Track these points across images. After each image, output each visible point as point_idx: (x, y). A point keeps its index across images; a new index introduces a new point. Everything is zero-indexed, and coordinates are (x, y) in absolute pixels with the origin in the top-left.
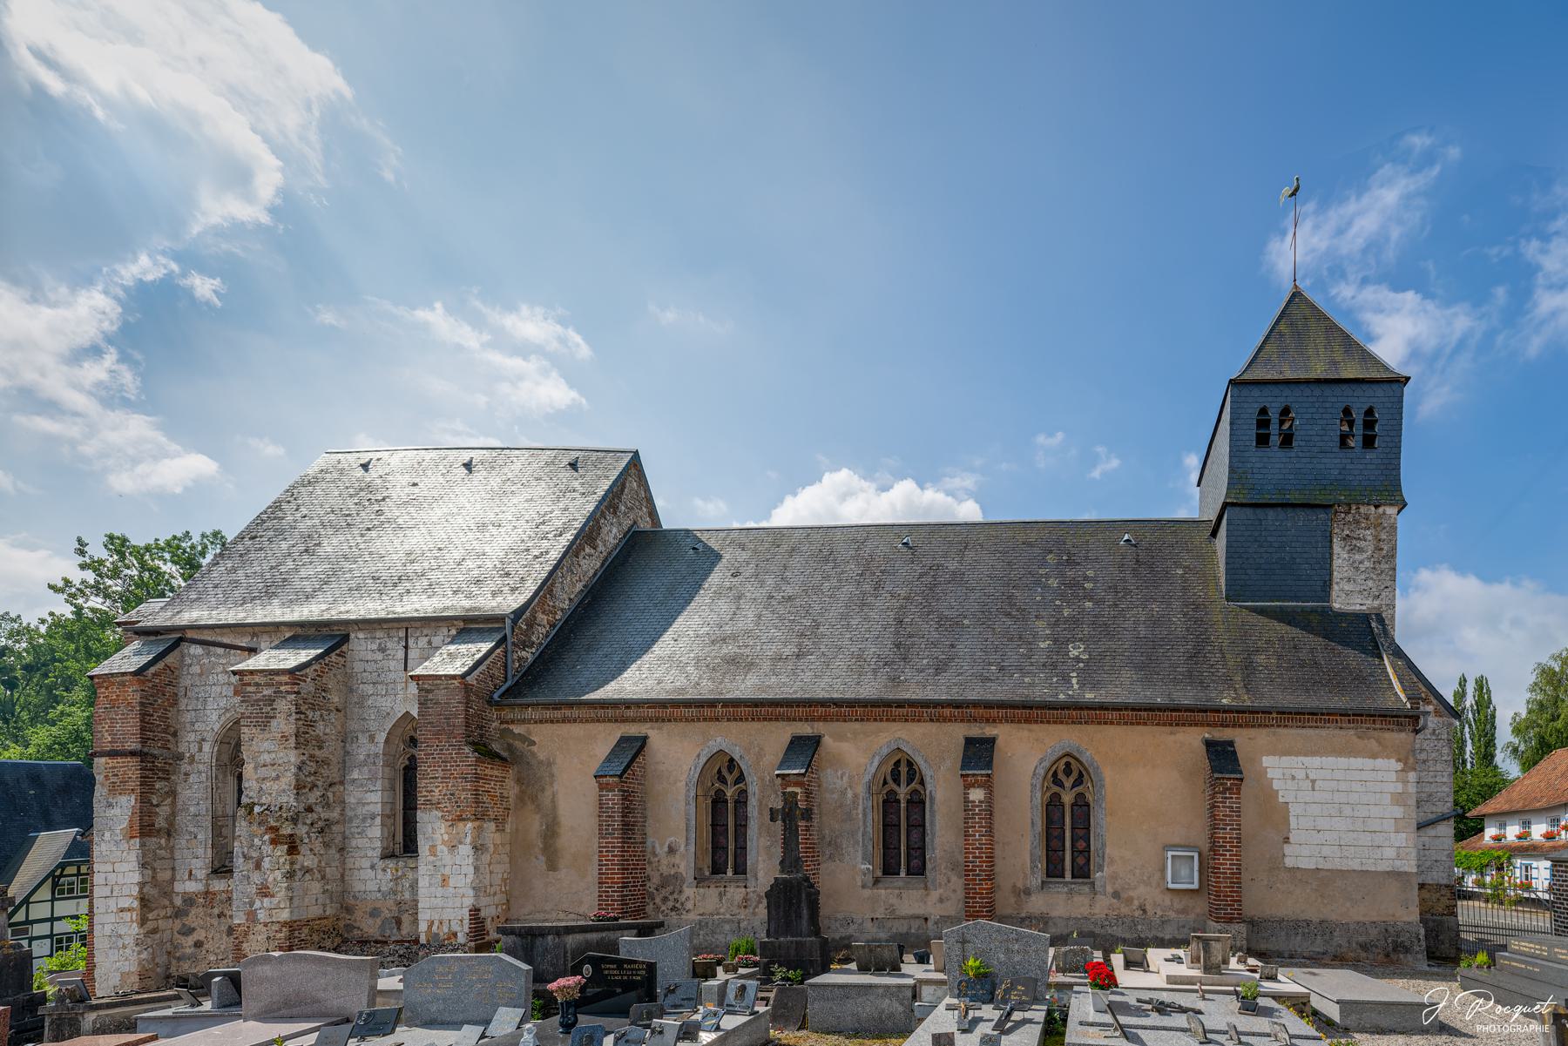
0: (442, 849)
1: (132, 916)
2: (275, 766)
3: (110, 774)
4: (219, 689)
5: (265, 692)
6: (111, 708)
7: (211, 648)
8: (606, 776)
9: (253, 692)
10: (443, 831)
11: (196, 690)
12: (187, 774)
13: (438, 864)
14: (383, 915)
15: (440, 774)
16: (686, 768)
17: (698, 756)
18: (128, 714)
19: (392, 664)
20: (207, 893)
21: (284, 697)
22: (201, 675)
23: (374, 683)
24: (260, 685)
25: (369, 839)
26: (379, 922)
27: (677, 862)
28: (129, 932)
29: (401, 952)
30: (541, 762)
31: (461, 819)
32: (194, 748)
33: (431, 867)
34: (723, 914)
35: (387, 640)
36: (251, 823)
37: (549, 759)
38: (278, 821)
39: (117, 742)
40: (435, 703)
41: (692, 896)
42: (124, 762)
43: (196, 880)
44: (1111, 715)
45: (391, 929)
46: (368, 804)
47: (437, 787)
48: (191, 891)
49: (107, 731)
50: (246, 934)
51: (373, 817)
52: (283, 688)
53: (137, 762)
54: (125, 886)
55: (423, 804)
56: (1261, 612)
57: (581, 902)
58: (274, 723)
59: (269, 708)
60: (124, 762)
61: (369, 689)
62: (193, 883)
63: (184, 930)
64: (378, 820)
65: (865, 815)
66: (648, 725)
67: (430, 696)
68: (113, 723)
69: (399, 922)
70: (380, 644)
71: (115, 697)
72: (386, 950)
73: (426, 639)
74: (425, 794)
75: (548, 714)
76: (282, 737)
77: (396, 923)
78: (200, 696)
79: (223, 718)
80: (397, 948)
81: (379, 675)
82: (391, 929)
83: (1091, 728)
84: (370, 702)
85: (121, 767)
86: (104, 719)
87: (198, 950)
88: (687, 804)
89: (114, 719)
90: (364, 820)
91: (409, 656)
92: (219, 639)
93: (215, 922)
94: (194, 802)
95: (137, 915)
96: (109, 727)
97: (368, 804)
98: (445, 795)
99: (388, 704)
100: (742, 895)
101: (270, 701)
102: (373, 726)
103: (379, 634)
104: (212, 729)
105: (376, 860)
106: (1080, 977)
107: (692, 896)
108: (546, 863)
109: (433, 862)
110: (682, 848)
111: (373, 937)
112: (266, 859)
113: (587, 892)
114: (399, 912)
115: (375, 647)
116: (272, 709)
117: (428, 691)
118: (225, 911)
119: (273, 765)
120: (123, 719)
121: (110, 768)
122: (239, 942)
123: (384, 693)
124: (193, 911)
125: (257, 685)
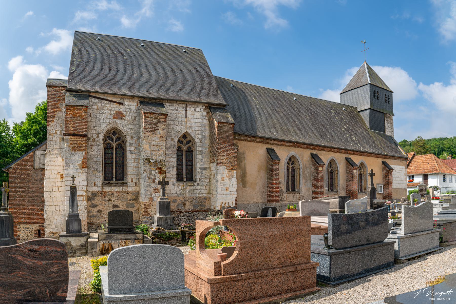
0: (226, 179)
1: (83, 199)
2: (158, 146)
3: (73, 143)
4: (106, 116)
5: (154, 121)
6: (73, 118)
7: (102, 100)
8: (276, 160)
9: (149, 120)
10: (227, 173)
11: (96, 115)
12: (92, 146)
13: (224, 183)
14: (178, 202)
15: (225, 154)
16: (284, 159)
17: (287, 156)
18: (81, 121)
19: (181, 115)
20: (102, 191)
21: (162, 123)
22: (97, 109)
23: (173, 121)
24: (153, 118)
25: (172, 174)
26: (176, 204)
27: (282, 186)
28: (82, 205)
29: (187, 215)
30: (241, 153)
31: (233, 169)
32: (95, 136)
33: (222, 185)
34: (294, 202)
35: (178, 107)
36: (150, 166)
37: (243, 152)
38: (162, 166)
39: (76, 131)
40: (223, 131)
41: (286, 196)
42: (80, 139)
43: (98, 186)
44: (370, 155)
45: (182, 207)
46: (171, 162)
47: (224, 158)
48: (95, 190)
49: (72, 126)
50: (149, 206)
51: (173, 167)
52: (161, 120)
53: (85, 139)
54: (80, 186)
55: (219, 164)
56: (376, 133)
57: (254, 198)
58: (158, 131)
59: (156, 126)
60: (80, 139)
61: (172, 123)
62: (96, 188)
63: (92, 205)
64: (175, 168)
65: (326, 175)
66: (274, 146)
67: (222, 129)
68: (75, 123)
69: (184, 205)
70: (175, 108)
71: (75, 114)
72: (182, 214)
73: (194, 108)
74: (220, 160)
75: (246, 138)
76: (161, 136)
77: (183, 205)
78: (97, 117)
79: (108, 126)
80: (186, 213)
81: (175, 118)
82: (182, 207)
83: (366, 157)
84: (172, 127)
85: (78, 140)
86: (70, 122)
87: (99, 214)
88: (285, 170)
89: (75, 122)
90: (170, 168)
91: (187, 113)
92: (106, 98)
93: (107, 203)
94: (95, 156)
95: (86, 198)
96: (72, 125)
97: (171, 162)
98: (227, 161)
99: (179, 128)
100: (299, 196)
101: (156, 124)
102: (173, 135)
103: (175, 105)
104: (103, 129)
105: (175, 182)
106: (9, 239)
107: (286, 196)
108: (242, 185)
109: (223, 183)
110: (283, 182)
111: (174, 210)
112: (156, 179)
113: (255, 195)
114: (185, 201)
115: (173, 109)
116: (157, 127)
117: (221, 127)
118: (111, 199)
119: (157, 146)
120: (79, 122)
121: (73, 140)
122: (147, 209)
123: (177, 124)
124: (96, 198)
125: (151, 118)
